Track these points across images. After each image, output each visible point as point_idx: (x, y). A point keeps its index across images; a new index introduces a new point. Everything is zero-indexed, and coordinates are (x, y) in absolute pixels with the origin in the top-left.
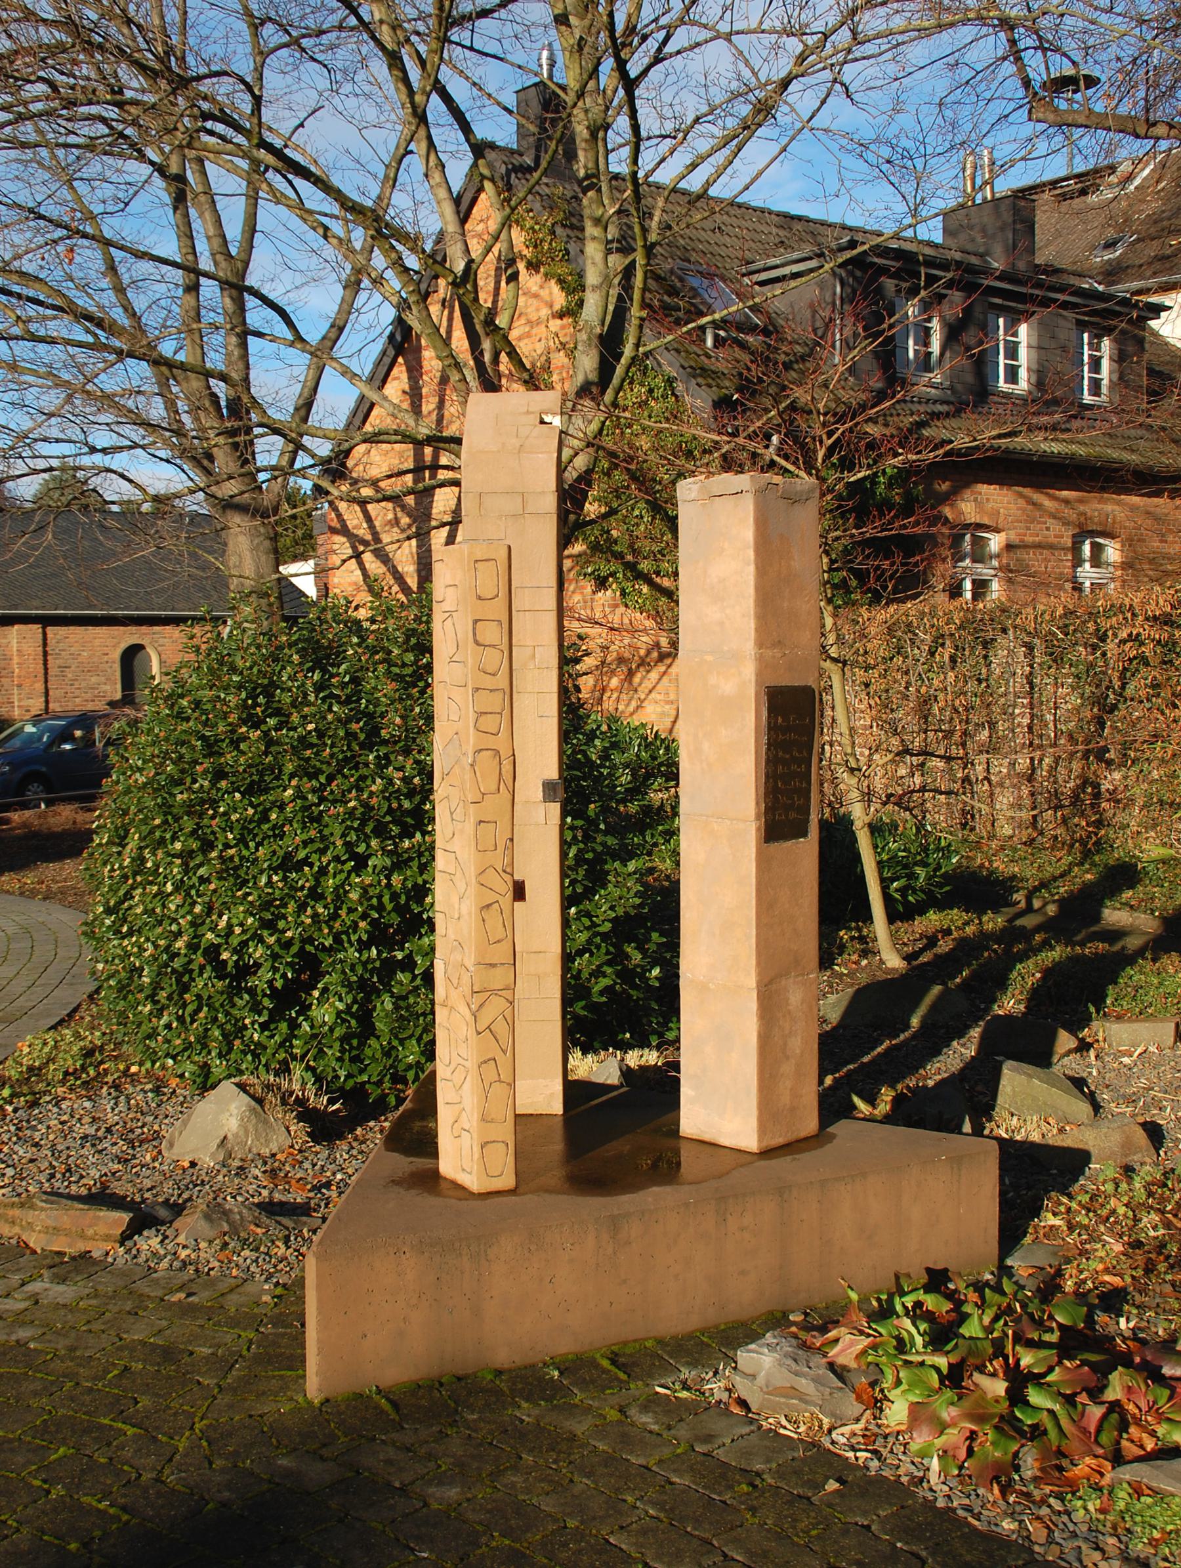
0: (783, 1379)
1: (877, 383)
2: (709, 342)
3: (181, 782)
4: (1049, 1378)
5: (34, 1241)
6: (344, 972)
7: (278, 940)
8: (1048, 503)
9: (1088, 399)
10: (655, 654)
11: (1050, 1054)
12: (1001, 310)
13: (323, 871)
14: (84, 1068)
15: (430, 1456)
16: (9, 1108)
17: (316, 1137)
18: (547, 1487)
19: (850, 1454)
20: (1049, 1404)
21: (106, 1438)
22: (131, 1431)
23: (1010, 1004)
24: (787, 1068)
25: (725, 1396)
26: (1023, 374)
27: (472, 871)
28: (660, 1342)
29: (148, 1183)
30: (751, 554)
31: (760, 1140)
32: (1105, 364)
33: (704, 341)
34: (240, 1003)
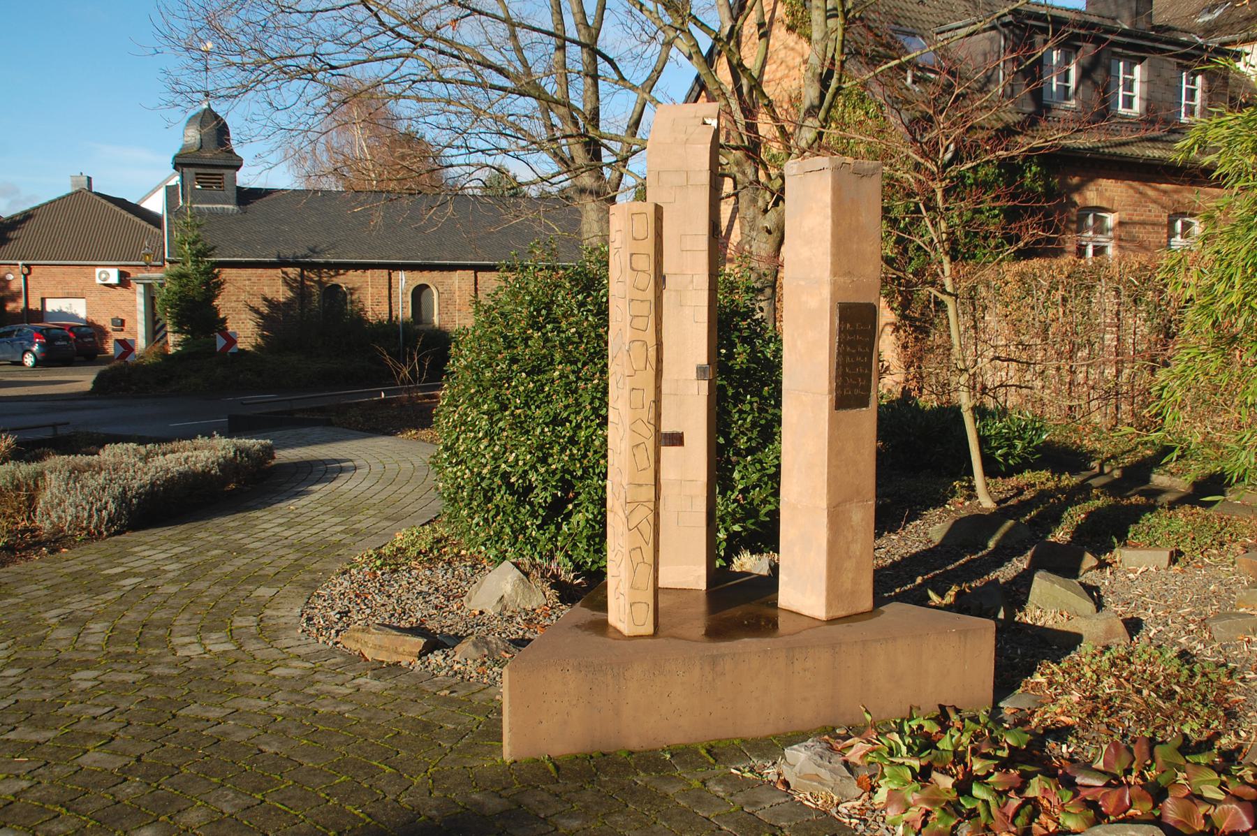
0: (812, 769)
1: (1029, 108)
2: (909, 80)
3: (490, 366)
4: (991, 779)
5: (369, 654)
6: (589, 493)
7: (547, 471)
8: (1151, 193)
9: (1184, 119)
11: (1078, 568)
12: (1121, 57)
13: (578, 426)
14: (431, 550)
15: (569, 801)
16: (379, 573)
17: (563, 599)
18: (637, 825)
19: (847, 820)
20: (985, 797)
21: (372, 772)
22: (388, 770)
23: (1061, 535)
24: (849, 564)
25: (775, 778)
27: (627, 422)
28: (744, 741)
29: (449, 622)
30: (829, 211)
31: (827, 612)
32: (1198, 94)
33: (905, 79)
34: (523, 511)
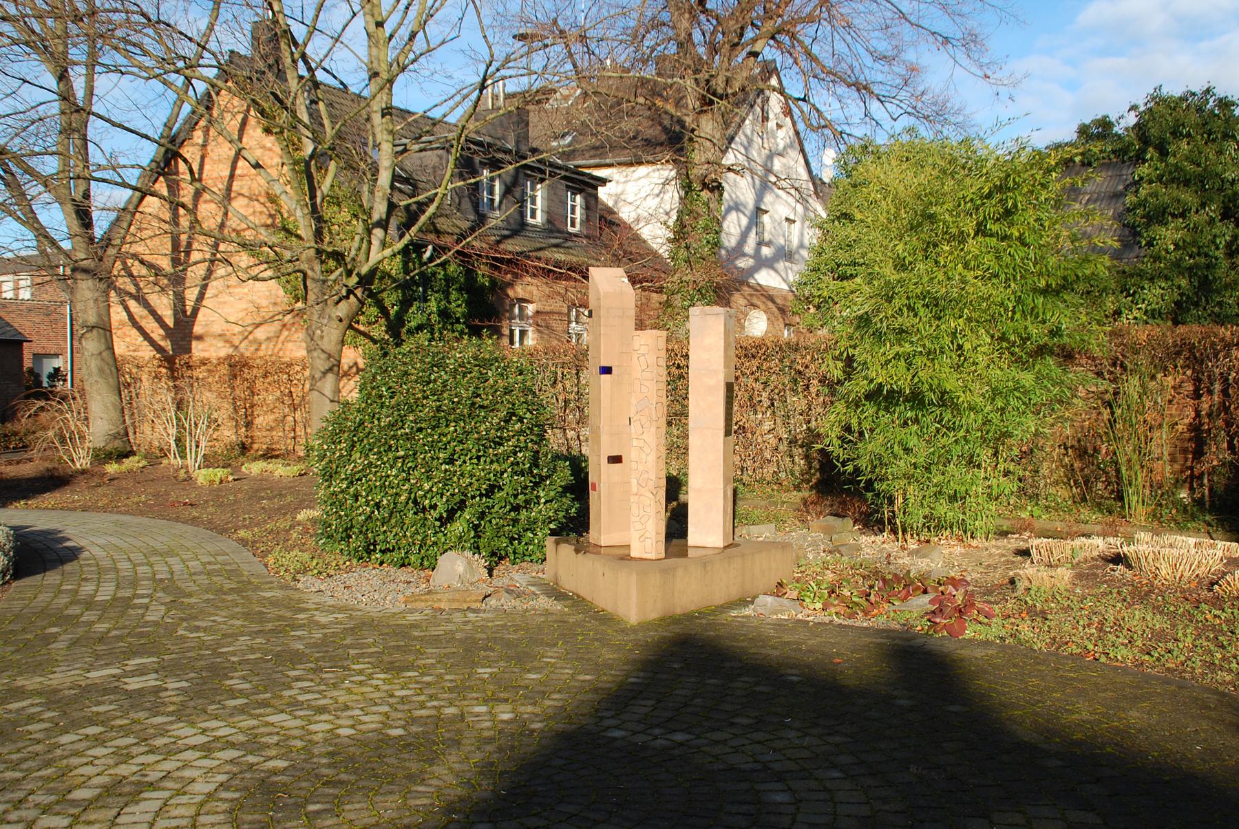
9: (570, 229)
10: (354, 369)
26: (539, 213)
